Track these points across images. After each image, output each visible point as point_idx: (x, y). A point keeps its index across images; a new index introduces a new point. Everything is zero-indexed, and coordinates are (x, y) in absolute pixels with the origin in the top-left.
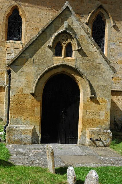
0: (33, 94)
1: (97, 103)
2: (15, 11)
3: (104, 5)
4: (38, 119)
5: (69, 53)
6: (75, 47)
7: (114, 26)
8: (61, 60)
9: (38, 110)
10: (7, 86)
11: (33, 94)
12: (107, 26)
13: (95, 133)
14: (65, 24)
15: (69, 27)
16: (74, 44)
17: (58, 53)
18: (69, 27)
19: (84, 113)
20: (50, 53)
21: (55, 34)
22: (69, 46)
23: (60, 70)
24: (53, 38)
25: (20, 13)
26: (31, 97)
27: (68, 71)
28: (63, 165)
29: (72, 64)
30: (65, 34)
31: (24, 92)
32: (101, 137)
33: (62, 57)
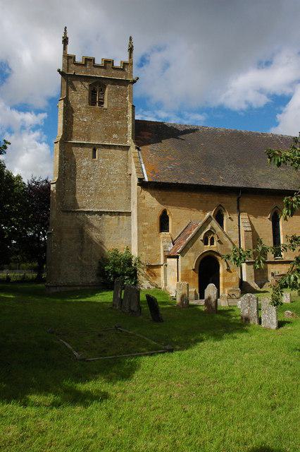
0: (193, 270)
1: (231, 272)
2: (164, 212)
3: (223, 205)
4: (197, 285)
5: (212, 243)
6: (216, 240)
7: (230, 218)
8: (208, 247)
9: (197, 279)
10: (78, 222)
11: (193, 270)
12: (225, 218)
13: (231, 291)
14: (209, 226)
15: (212, 228)
16: (215, 237)
17: (206, 243)
18: (212, 228)
19: (224, 279)
20: (202, 244)
21: (204, 232)
22: (212, 239)
23: (208, 254)
24: (203, 234)
25: (168, 213)
26: (192, 271)
27: (212, 254)
28: (282, 329)
29: (214, 250)
30: (210, 232)
31: (189, 269)
32: (234, 293)
33: (209, 245)
